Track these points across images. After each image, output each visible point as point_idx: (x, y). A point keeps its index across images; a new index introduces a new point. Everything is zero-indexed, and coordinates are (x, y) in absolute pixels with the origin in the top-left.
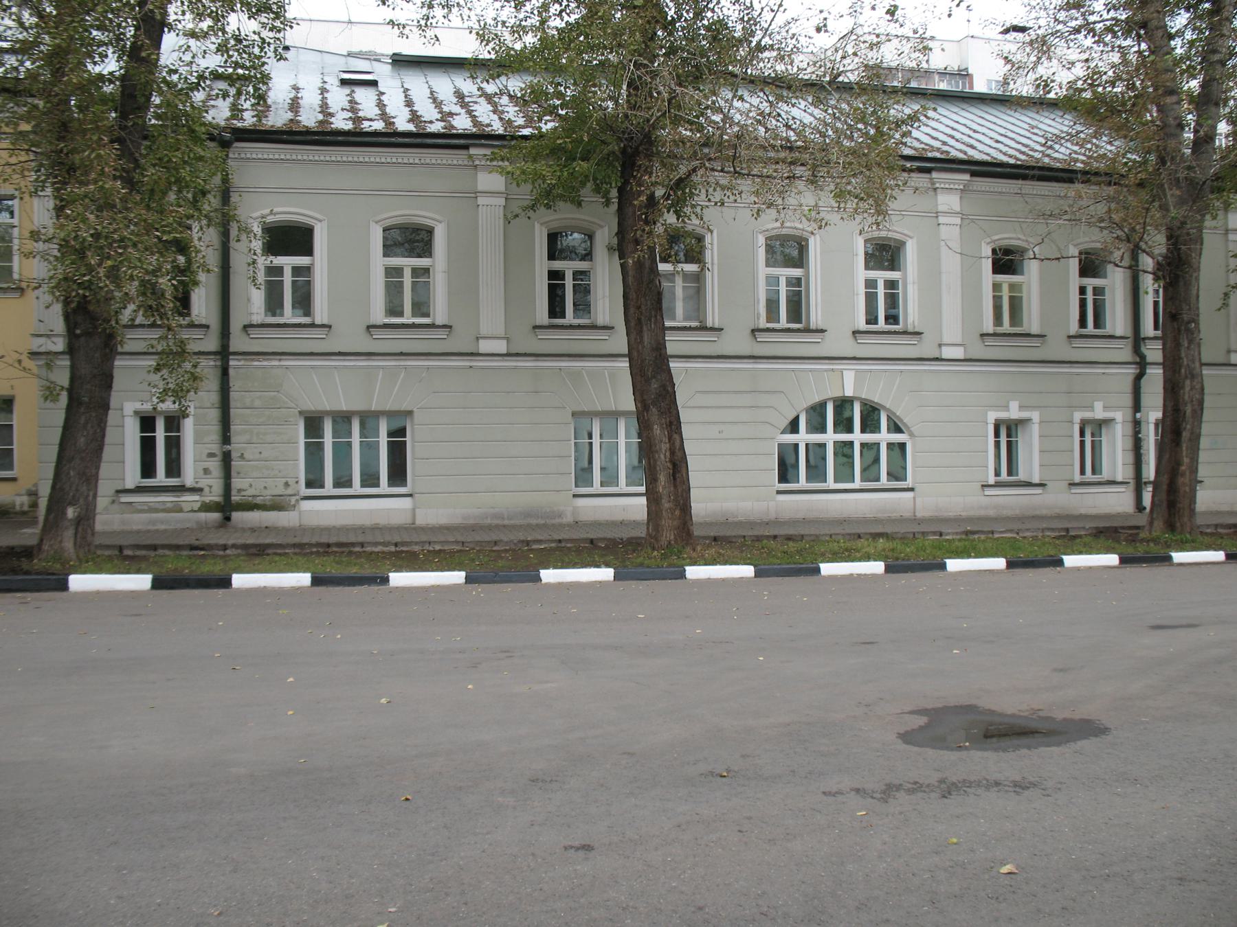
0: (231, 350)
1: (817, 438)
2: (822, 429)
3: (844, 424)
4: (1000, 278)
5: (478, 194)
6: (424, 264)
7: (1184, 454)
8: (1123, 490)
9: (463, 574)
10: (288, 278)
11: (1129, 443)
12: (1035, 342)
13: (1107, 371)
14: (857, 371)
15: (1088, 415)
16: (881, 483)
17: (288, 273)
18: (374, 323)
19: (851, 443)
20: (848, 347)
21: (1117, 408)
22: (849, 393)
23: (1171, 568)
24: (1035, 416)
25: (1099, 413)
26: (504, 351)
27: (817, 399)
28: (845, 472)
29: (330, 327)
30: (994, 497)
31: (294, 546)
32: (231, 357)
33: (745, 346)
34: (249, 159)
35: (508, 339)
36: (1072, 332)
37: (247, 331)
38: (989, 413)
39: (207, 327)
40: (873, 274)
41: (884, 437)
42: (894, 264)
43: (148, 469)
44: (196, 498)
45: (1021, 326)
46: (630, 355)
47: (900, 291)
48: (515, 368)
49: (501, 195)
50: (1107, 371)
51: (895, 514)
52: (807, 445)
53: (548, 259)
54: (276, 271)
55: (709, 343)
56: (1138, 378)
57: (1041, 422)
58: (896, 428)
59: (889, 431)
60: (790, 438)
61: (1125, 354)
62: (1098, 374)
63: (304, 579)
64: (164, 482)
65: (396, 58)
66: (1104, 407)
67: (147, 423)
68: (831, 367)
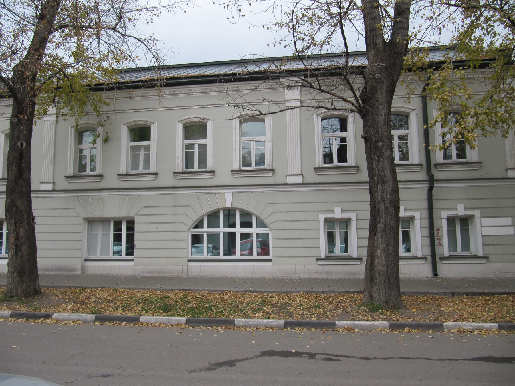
2: (233, 226)
5: (285, 101)
6: (204, 142)
7: (380, 240)
10: (196, 150)
11: (426, 232)
12: (210, 175)
13: (220, 191)
14: (233, 193)
15: (330, 216)
17: (196, 147)
18: (439, 162)
20: (229, 179)
21: (417, 209)
22: (229, 205)
24: (353, 216)
25: (461, 211)
26: (301, 182)
28: (230, 250)
30: (325, 266)
32: (435, 182)
33: (170, 181)
37: (436, 167)
38: (443, 213)
39: (422, 165)
41: (254, 230)
45: (194, 168)
47: (185, 151)
48: (57, 197)
49: (297, 101)
50: (38, 196)
52: (257, 234)
54: (189, 147)
55: (150, 181)
56: (430, 189)
57: (357, 220)
58: (261, 224)
59: (258, 226)
61: (422, 175)
66: (405, 209)
67: (451, 221)
68: (218, 191)
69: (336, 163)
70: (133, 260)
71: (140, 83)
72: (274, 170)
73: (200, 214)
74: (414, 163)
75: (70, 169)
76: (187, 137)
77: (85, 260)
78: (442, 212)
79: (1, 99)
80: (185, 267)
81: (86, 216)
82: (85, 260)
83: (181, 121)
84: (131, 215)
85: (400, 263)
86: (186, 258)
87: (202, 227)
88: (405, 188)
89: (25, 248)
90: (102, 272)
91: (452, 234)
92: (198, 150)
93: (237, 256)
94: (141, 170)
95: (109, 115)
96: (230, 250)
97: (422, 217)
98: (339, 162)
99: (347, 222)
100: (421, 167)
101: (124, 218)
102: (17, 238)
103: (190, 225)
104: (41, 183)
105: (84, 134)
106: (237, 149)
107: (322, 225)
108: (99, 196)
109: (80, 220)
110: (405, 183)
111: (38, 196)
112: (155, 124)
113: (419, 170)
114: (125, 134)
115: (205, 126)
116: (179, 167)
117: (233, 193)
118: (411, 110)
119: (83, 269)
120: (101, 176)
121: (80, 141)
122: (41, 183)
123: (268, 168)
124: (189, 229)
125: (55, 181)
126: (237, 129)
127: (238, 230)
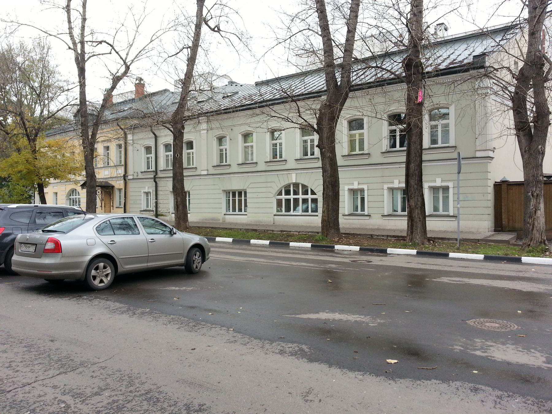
1: (305, 197)
8: (455, 220)
9: (310, 244)
12: (284, 163)
13: (401, 166)
22: (294, 181)
23: (386, 256)
24: (365, 187)
26: (206, 174)
27: (287, 182)
28: (288, 209)
31: (394, 236)
35: (207, 170)
36: (384, 150)
38: (345, 187)
40: (305, 138)
41: (310, 196)
42: (361, 127)
44: (153, 213)
46: (338, 167)
50: (401, 166)
57: (368, 190)
58: (313, 193)
60: (279, 197)
62: (397, 168)
63: (481, 257)
65: (257, 83)
68: (288, 173)
69: (359, 212)
70: (247, 215)
71: (441, 74)
73: (280, 186)
75: (216, 162)
76: (391, 124)
80: (272, 219)
81: (223, 189)
82: (224, 214)
84: (245, 188)
85: (426, 219)
89: (181, 207)
91: (436, 200)
92: (439, 130)
93: (237, 212)
94: (357, 152)
96: (288, 209)
98: (400, 147)
99: (446, 189)
101: (237, 190)
102: (177, 202)
103: (274, 193)
105: (223, 139)
107: (386, 192)
108: (229, 177)
109: (221, 192)
114: (240, 138)
119: (224, 219)
124: (274, 196)
127: (301, 197)
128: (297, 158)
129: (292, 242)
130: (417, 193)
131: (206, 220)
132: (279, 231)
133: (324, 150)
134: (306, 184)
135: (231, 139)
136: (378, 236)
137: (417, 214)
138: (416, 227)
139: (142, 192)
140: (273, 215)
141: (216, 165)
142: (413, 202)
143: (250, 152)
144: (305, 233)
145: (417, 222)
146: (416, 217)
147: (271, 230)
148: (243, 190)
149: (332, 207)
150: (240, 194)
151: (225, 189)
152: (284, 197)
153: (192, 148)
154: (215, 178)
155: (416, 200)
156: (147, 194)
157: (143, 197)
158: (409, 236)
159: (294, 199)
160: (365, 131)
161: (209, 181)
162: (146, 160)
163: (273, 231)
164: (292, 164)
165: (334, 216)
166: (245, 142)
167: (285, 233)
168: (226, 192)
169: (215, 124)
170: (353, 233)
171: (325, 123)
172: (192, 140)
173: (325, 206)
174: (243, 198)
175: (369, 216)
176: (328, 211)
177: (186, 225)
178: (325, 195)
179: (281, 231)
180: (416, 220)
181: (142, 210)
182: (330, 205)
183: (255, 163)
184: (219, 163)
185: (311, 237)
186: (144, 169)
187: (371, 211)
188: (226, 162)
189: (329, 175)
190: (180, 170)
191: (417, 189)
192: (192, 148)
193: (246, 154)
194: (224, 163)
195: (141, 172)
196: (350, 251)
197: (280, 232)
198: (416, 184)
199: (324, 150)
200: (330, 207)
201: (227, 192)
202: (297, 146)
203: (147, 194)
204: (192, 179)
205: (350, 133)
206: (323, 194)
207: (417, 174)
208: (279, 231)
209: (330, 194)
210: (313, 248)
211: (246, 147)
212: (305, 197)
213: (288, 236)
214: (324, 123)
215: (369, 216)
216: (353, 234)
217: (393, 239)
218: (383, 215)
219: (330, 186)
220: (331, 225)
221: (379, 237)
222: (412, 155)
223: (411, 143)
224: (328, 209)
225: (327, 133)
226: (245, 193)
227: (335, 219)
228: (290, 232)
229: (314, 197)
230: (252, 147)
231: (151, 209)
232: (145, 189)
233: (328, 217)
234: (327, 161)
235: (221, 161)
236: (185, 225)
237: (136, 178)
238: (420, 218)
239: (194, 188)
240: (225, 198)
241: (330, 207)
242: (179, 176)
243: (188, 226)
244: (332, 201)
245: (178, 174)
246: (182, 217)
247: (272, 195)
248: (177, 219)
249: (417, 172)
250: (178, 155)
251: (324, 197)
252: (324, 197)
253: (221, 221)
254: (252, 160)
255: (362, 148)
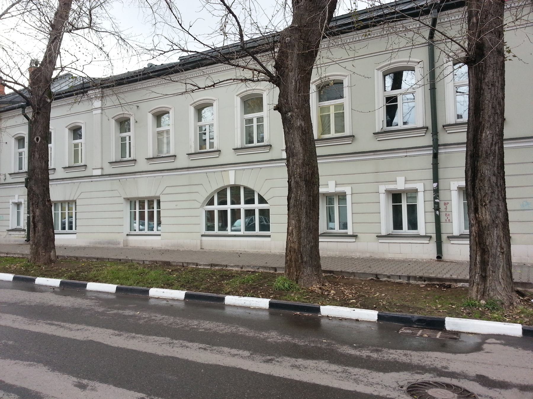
0: (440, 142)
3: (236, 200)
4: (124, 135)
12: (216, 155)
13: (408, 154)
14: (235, 170)
16: (270, 232)
19: (253, 211)
22: (232, 183)
24: (347, 190)
26: (100, 174)
27: (220, 185)
28: (224, 227)
29: (175, 156)
34: (443, 22)
35: (102, 169)
36: (378, 130)
40: (249, 116)
41: (257, 206)
43: (398, 225)
46: (316, 156)
49: (98, 109)
50: (408, 154)
51: (261, 250)
53: (161, 127)
56: (435, 156)
57: (352, 194)
58: (262, 200)
60: (210, 208)
61: (428, 140)
62: (401, 157)
64: (139, 233)
68: (223, 169)
70: (160, 235)
72: (55, 169)
74: (418, 127)
75: (114, 155)
76: (246, 112)
77: (127, 235)
78: (451, 182)
79: (1, 114)
80: (199, 242)
81: (126, 197)
82: (127, 235)
83: (114, 117)
84: (157, 195)
86: (200, 233)
87: (213, 204)
88: (406, 156)
90: (139, 245)
94: (333, 134)
95: (138, 105)
97: (426, 189)
100: (426, 131)
101: (146, 198)
104: (93, 169)
106: (238, 127)
107: (383, 198)
108: (134, 178)
109: (122, 200)
110: (405, 151)
111: (92, 180)
112: (173, 109)
113: (424, 134)
114: (150, 118)
115: (261, 99)
116: (192, 148)
117: (235, 170)
118: (415, 64)
119: (126, 242)
120: (352, 137)
121: (200, 118)
122: (93, 169)
123: (348, 135)
124: (202, 206)
125: (103, 167)
126: (238, 108)
127: (243, 206)
128: (236, 147)
129: (228, 294)
130: (496, 192)
131: (100, 243)
132: (208, 265)
133: (290, 114)
134: (251, 186)
135: (136, 122)
136: (389, 277)
137: (496, 238)
138: (494, 266)
139: (11, 203)
140: (200, 235)
141: (114, 161)
142: (488, 214)
143: (165, 140)
144: (253, 270)
145: (495, 257)
146: (495, 244)
147: (193, 264)
148: (155, 197)
149: (307, 223)
150: (151, 202)
151: (128, 197)
152: (216, 207)
153: (80, 137)
154: (113, 180)
155: (495, 209)
156: (18, 205)
157: (13, 210)
158: (478, 284)
159: (233, 211)
160: (346, 101)
161: (105, 184)
162: (18, 157)
163: (197, 265)
164: (228, 156)
165: (310, 242)
166: (159, 125)
167: (217, 268)
168: (131, 202)
169: (112, 100)
170: (339, 270)
171: (292, 62)
172: (80, 124)
173: (293, 222)
174: (155, 210)
175: (355, 236)
176: (299, 232)
177: (50, 256)
178: (292, 201)
179: (212, 265)
180: (494, 251)
181: (10, 228)
182: (304, 219)
183: (53, 169)
184: (119, 158)
185: (265, 278)
186: (14, 169)
187: (358, 230)
188: (130, 156)
189: (300, 161)
190: (42, 163)
191: (497, 185)
192: (80, 137)
193: (159, 143)
194: (128, 158)
195: (10, 174)
196: (357, 320)
197: (209, 267)
198: (494, 175)
199: (290, 114)
200: (303, 225)
201: (131, 201)
202: (237, 128)
203: (18, 205)
204: (80, 182)
205: (321, 105)
206: (289, 199)
207: (497, 152)
208: (208, 265)
209: (303, 198)
210: (273, 310)
211: (160, 133)
212: (250, 206)
213: (222, 276)
214: (290, 62)
215: (355, 236)
216: (341, 272)
217: (422, 284)
218: (379, 235)
219: (302, 184)
220: (305, 259)
221: (392, 280)
222: (486, 111)
223: (484, 86)
224: (300, 227)
225: (296, 82)
226: (159, 202)
227: (312, 247)
228: (226, 266)
229: (264, 206)
230: (168, 132)
231: (23, 228)
232: (15, 199)
233: (300, 243)
234: (297, 136)
235: (123, 154)
236: (47, 256)
237: (4, 182)
238: (502, 248)
239: (82, 196)
240: (129, 210)
241: (303, 225)
242: (39, 173)
243: (53, 258)
244: (306, 212)
245: (37, 170)
246: (41, 243)
247: (199, 205)
248: (34, 246)
249: (497, 148)
250: (37, 139)
251: (292, 205)
252: (292, 205)
253: (121, 245)
254: (168, 152)
255: (340, 127)
